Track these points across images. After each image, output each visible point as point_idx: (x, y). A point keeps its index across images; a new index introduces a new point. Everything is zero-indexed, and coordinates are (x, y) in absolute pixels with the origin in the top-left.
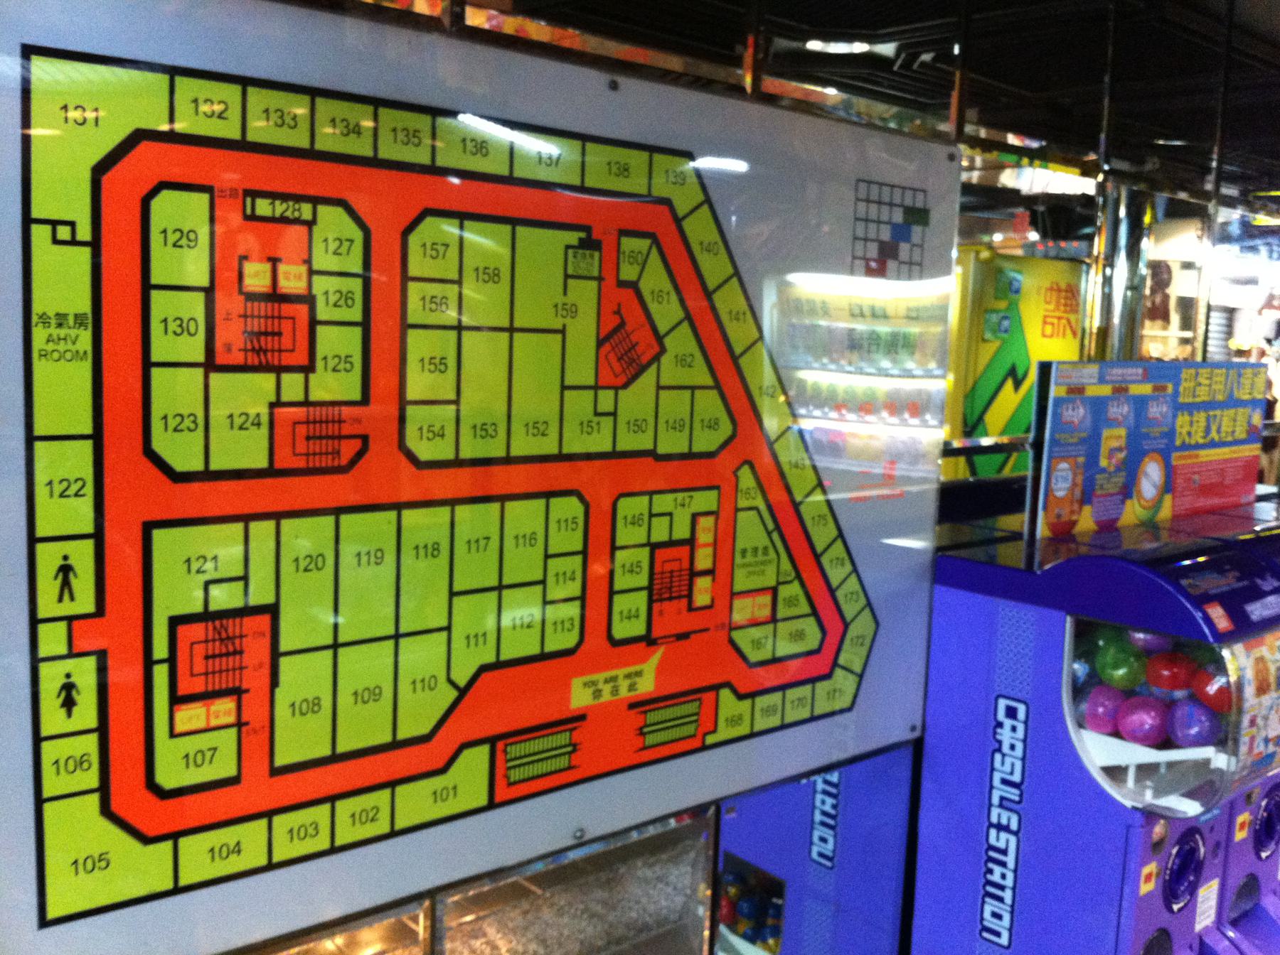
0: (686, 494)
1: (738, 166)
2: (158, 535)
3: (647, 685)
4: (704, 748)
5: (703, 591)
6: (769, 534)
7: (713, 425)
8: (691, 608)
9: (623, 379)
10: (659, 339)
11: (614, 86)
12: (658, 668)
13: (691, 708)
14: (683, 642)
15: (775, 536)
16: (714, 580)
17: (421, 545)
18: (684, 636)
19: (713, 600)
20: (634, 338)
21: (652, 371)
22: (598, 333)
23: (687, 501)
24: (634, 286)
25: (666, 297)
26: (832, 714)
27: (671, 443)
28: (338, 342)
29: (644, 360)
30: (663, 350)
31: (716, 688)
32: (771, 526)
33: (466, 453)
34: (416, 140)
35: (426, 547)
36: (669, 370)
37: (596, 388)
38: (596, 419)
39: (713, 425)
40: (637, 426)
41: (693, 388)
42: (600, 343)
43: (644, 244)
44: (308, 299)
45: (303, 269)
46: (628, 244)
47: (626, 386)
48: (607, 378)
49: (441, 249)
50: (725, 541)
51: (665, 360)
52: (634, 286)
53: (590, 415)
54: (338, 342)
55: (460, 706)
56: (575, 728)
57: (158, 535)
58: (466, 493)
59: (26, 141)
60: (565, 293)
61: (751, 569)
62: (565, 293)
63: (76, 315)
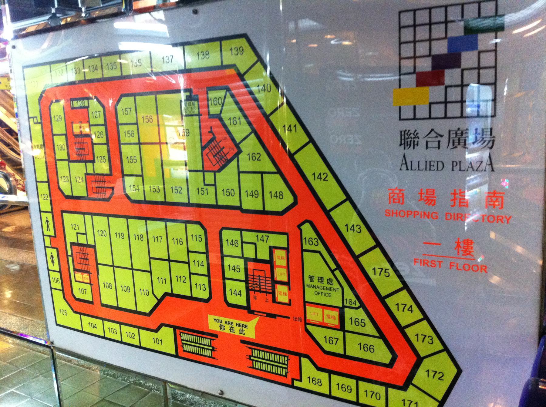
0: (264, 234)
1: (316, 45)
3: (250, 333)
4: (292, 386)
5: (282, 294)
6: (332, 271)
7: (280, 196)
8: (274, 300)
9: (217, 167)
10: (237, 146)
11: (195, 12)
12: (256, 327)
13: (283, 359)
14: (272, 319)
15: (337, 273)
16: (289, 289)
17: (155, 237)
18: (274, 316)
19: (290, 300)
20: (221, 144)
21: (234, 163)
23: (265, 238)
24: (218, 117)
25: (238, 121)
27: (249, 204)
28: (101, 151)
29: (229, 157)
30: (240, 151)
31: (300, 355)
32: (333, 266)
33: (193, 201)
34: (115, 67)
35: (196, 236)
36: (245, 163)
37: (203, 171)
38: (206, 187)
39: (280, 196)
40: (229, 193)
41: (262, 173)
42: (203, 148)
43: (222, 93)
44: (88, 136)
45: (87, 125)
46: (212, 95)
47: (220, 170)
48: (208, 164)
49: (129, 110)
50: (296, 266)
51: (240, 156)
52: (218, 117)
53: (202, 185)
54: (101, 151)
55: (373, 293)
56: (213, 340)
58: (133, 215)
61: (318, 290)
63: (427, 190)
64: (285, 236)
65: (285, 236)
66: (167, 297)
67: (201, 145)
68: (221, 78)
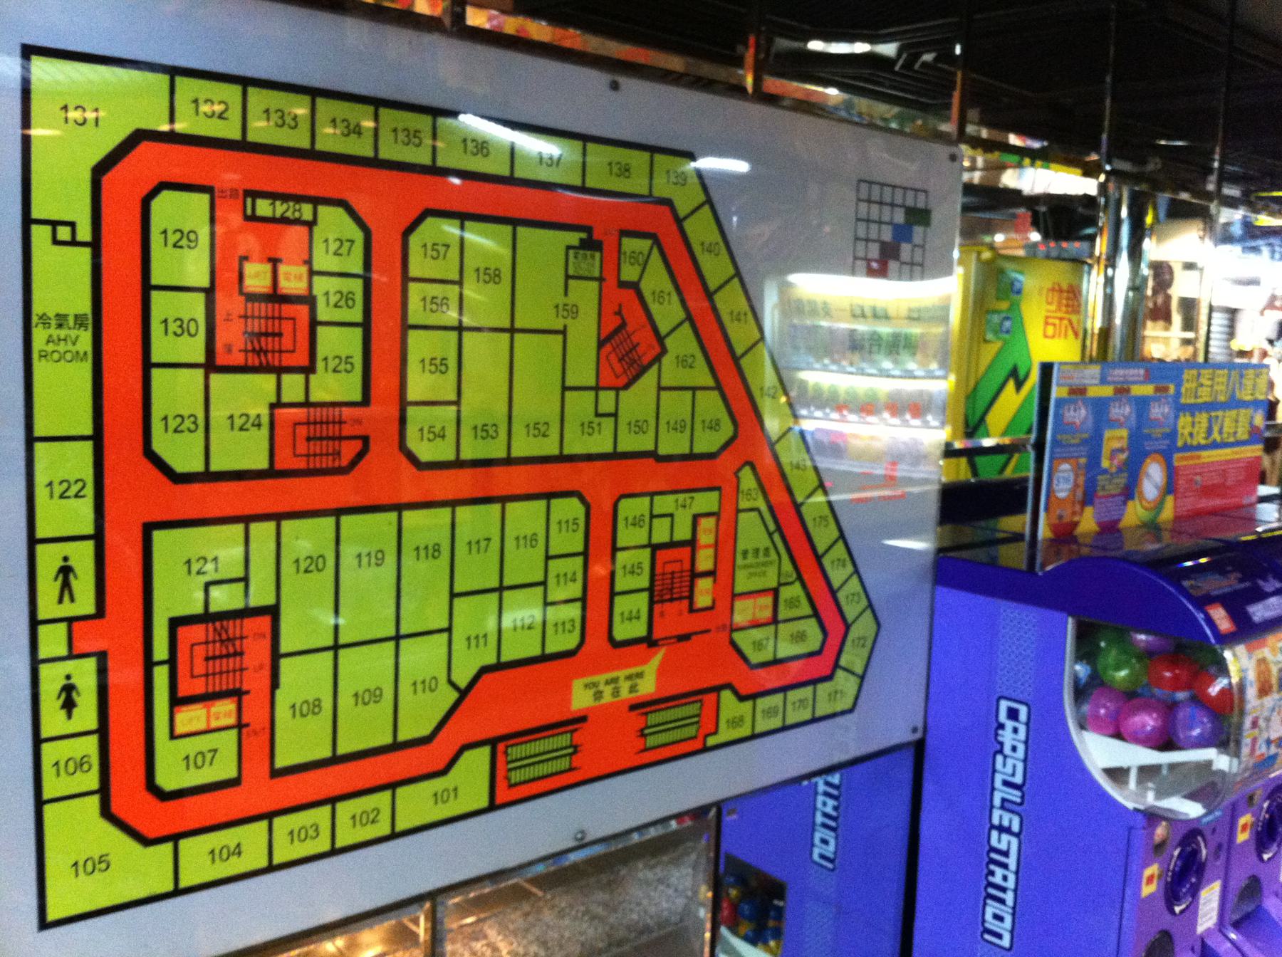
0: (687, 495)
1: (740, 166)
3: (648, 686)
4: (705, 749)
5: (704, 593)
6: (770, 535)
7: (714, 426)
8: (692, 610)
9: (624, 380)
10: (660, 339)
11: (615, 86)
12: (659, 670)
13: (692, 709)
14: (684, 643)
15: (777, 537)
16: (715, 581)
17: (422, 546)
18: (685, 637)
19: (714, 601)
20: (635, 339)
21: (653, 371)
23: (688, 502)
24: (635, 286)
25: (667, 298)
27: (672, 444)
28: (339, 343)
29: (645, 360)
30: (664, 351)
31: (717, 689)
32: (772, 527)
34: (417, 141)
36: (670, 371)
37: (596, 389)
38: (597, 420)
39: (714, 426)
40: (638, 427)
41: (694, 389)
42: (601, 344)
43: (645, 244)
44: (309, 300)
45: (304, 270)
46: (629, 244)
47: (627, 387)
48: (608, 379)
49: (442, 250)
50: (726, 542)
51: (666, 360)
52: (635, 286)
53: (591, 416)
54: (339, 343)
56: (576, 730)
58: (466, 494)
61: (752, 570)
64: (158, 536)
65: (158, 536)
66: (114, 808)
67: (599, 334)
68: (1213, 512)
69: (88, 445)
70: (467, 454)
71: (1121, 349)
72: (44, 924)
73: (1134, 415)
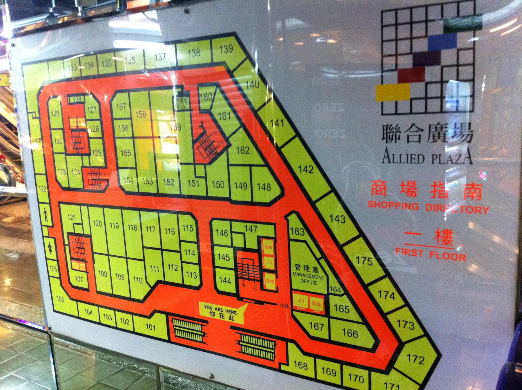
0: (253, 225)
2: (273, 227)
3: (239, 319)
4: (280, 370)
5: (270, 282)
6: (318, 260)
7: (267, 187)
8: (262, 288)
9: (208, 160)
10: (227, 139)
11: (187, 12)
12: (244, 314)
13: (271, 344)
14: (260, 306)
15: (322, 261)
16: (277, 277)
17: (149, 227)
18: (262, 303)
19: (277, 288)
20: (212, 138)
21: (224, 156)
22: (192, 139)
23: (254, 228)
24: (209, 112)
25: (228, 116)
26: (131, 113)
27: (238, 195)
28: (96, 145)
29: (219, 150)
30: (229, 145)
31: (287, 341)
32: (319, 255)
34: (110, 64)
35: (187, 226)
36: (235, 156)
37: (194, 164)
38: (197, 179)
39: (267, 187)
40: (219, 185)
41: (250, 166)
42: (194, 142)
43: (212, 89)
44: (85, 130)
45: (84, 119)
46: (203, 91)
47: (210, 163)
48: (199, 157)
49: (123, 105)
50: (283, 255)
51: (230, 150)
52: (209, 112)
53: (193, 177)
54: (96, 145)
56: (203, 325)
57: (273, 227)
58: (127, 206)
59: (157, 177)
60: (276, 304)
61: (304, 278)
62: (276, 304)
69: (314, 199)
70: (185, 192)
71: (303, 20)
72: (323, 325)
73: (488, 168)
